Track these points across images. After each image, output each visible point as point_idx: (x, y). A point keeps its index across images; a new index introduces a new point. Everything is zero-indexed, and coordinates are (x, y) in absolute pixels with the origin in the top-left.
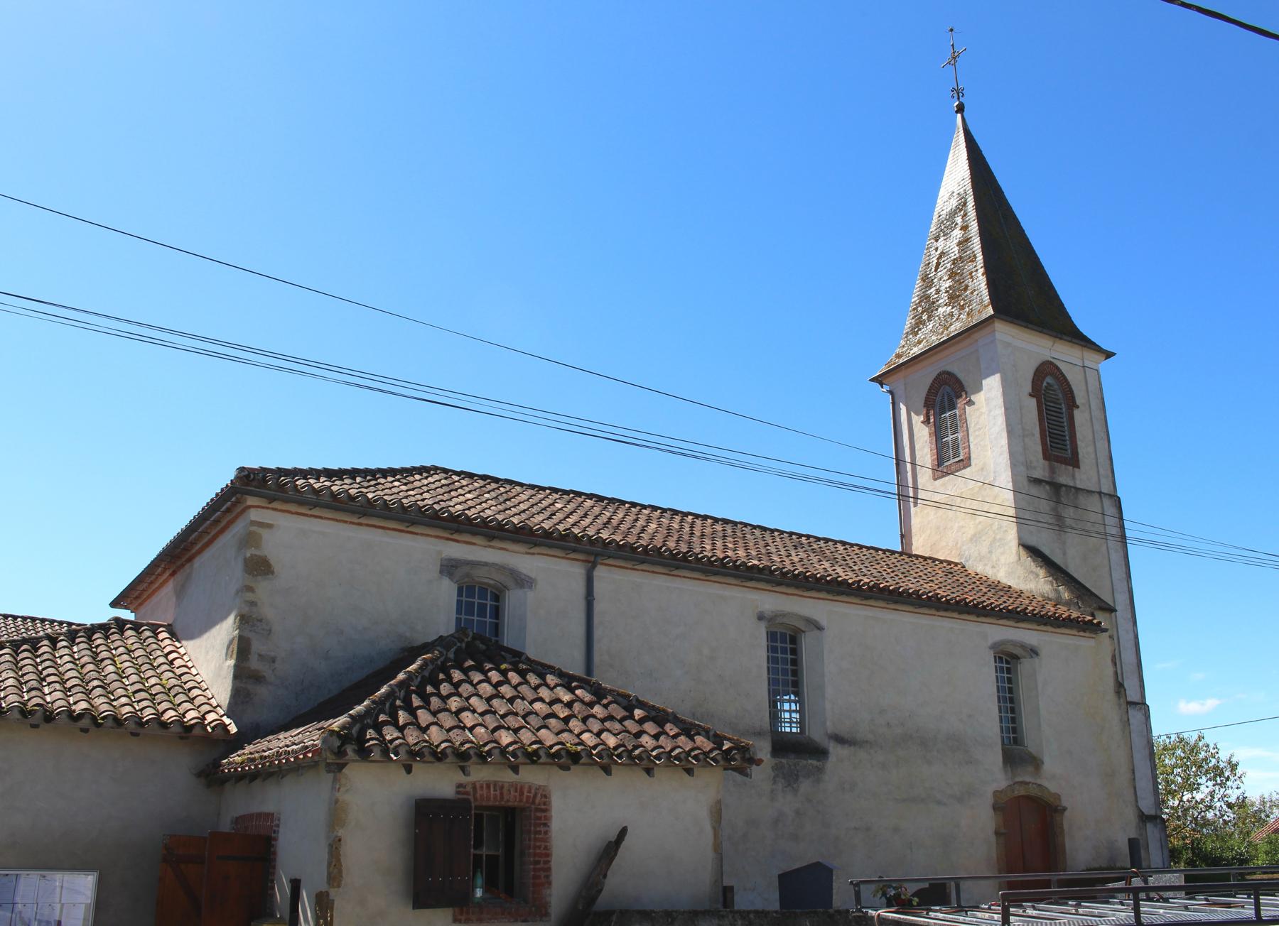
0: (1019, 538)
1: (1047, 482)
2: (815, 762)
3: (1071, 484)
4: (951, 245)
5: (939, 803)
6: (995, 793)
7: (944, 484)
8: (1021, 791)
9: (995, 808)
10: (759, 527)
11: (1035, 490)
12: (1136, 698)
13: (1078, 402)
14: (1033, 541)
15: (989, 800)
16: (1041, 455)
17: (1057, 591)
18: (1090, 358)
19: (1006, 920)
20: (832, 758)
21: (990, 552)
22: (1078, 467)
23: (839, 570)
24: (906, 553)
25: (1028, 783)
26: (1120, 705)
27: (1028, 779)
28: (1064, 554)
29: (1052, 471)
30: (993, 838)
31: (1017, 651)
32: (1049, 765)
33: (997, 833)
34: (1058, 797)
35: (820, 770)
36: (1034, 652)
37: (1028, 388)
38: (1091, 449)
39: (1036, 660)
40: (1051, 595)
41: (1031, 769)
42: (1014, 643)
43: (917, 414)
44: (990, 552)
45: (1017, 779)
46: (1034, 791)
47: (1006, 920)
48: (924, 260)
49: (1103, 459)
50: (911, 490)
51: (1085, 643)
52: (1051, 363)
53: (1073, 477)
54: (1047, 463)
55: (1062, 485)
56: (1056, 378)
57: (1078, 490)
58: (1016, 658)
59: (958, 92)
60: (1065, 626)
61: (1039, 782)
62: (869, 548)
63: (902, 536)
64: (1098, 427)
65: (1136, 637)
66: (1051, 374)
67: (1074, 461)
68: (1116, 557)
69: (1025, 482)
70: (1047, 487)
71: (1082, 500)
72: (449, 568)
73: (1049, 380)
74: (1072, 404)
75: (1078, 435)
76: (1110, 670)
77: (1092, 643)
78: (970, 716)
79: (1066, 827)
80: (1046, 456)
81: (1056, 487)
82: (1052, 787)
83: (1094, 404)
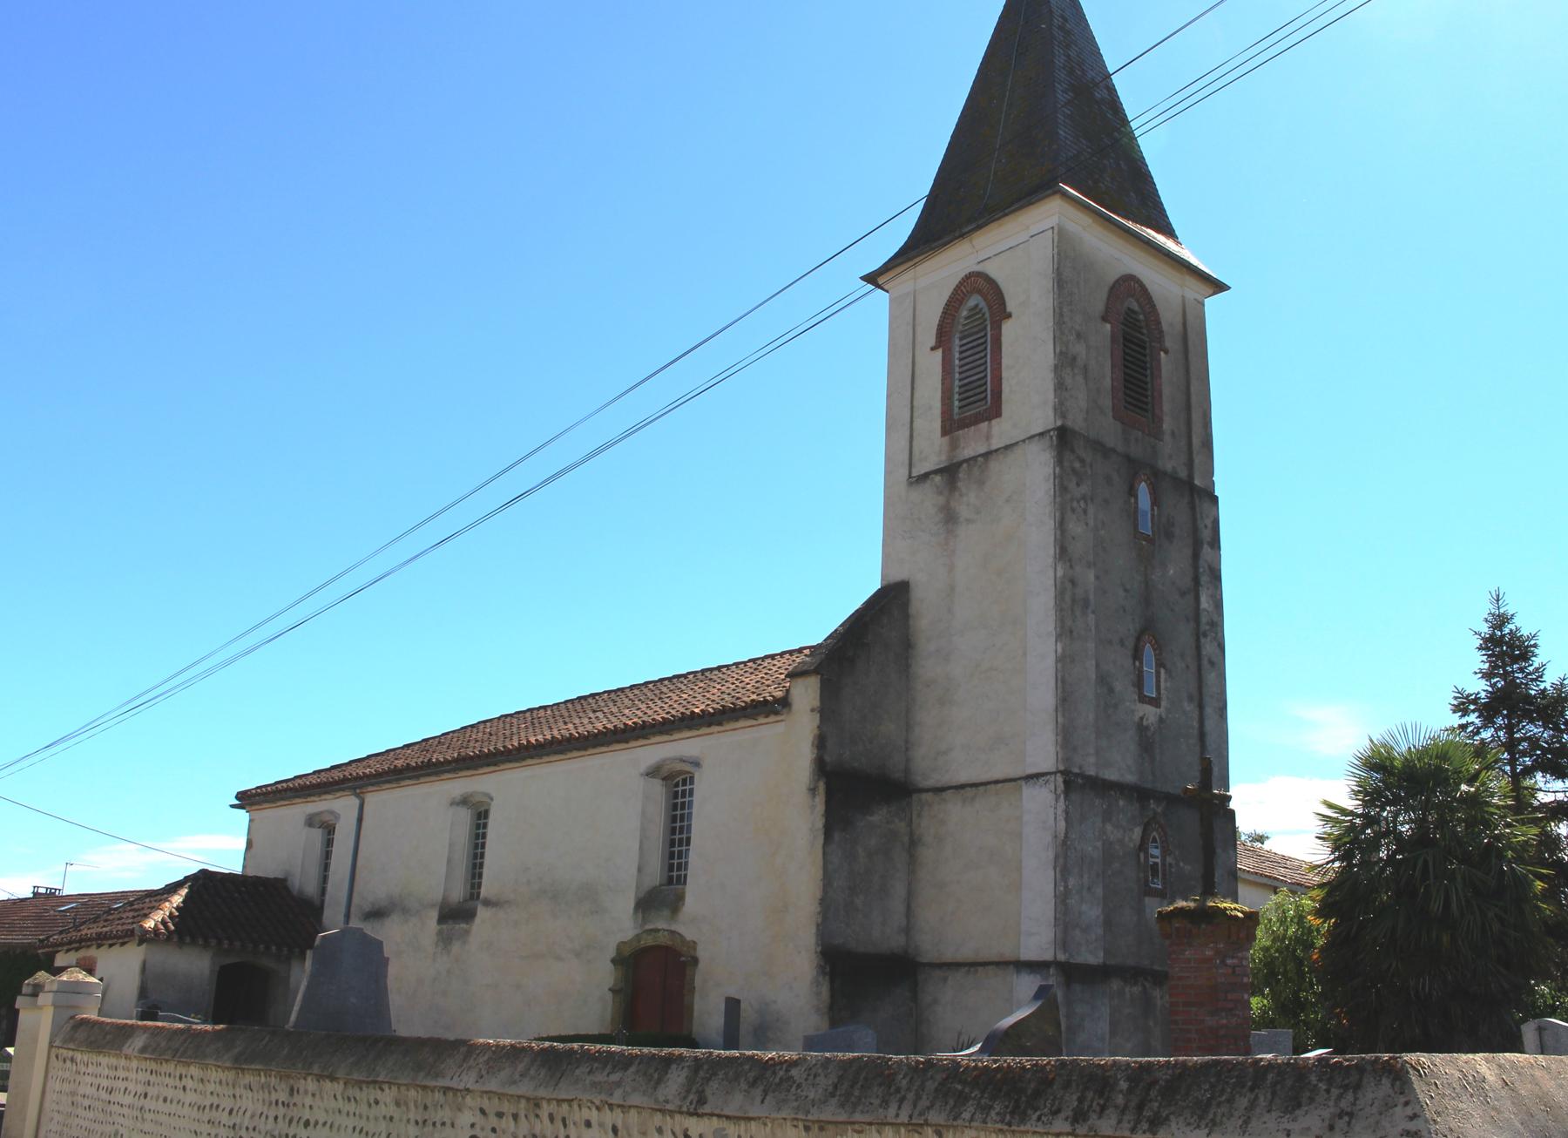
2: (464, 926)
5: (559, 958)
8: (649, 941)
10: (767, 657)
15: (612, 953)
19: (773, 1133)
20: (477, 920)
23: (624, 719)
25: (657, 930)
27: (661, 925)
30: (609, 996)
35: (467, 932)
41: (666, 912)
45: (648, 927)
46: (663, 939)
47: (773, 1133)
60: (679, 729)
62: (782, 654)
66: (979, 292)
72: (310, 821)
73: (974, 300)
77: (780, 728)
82: (688, 933)
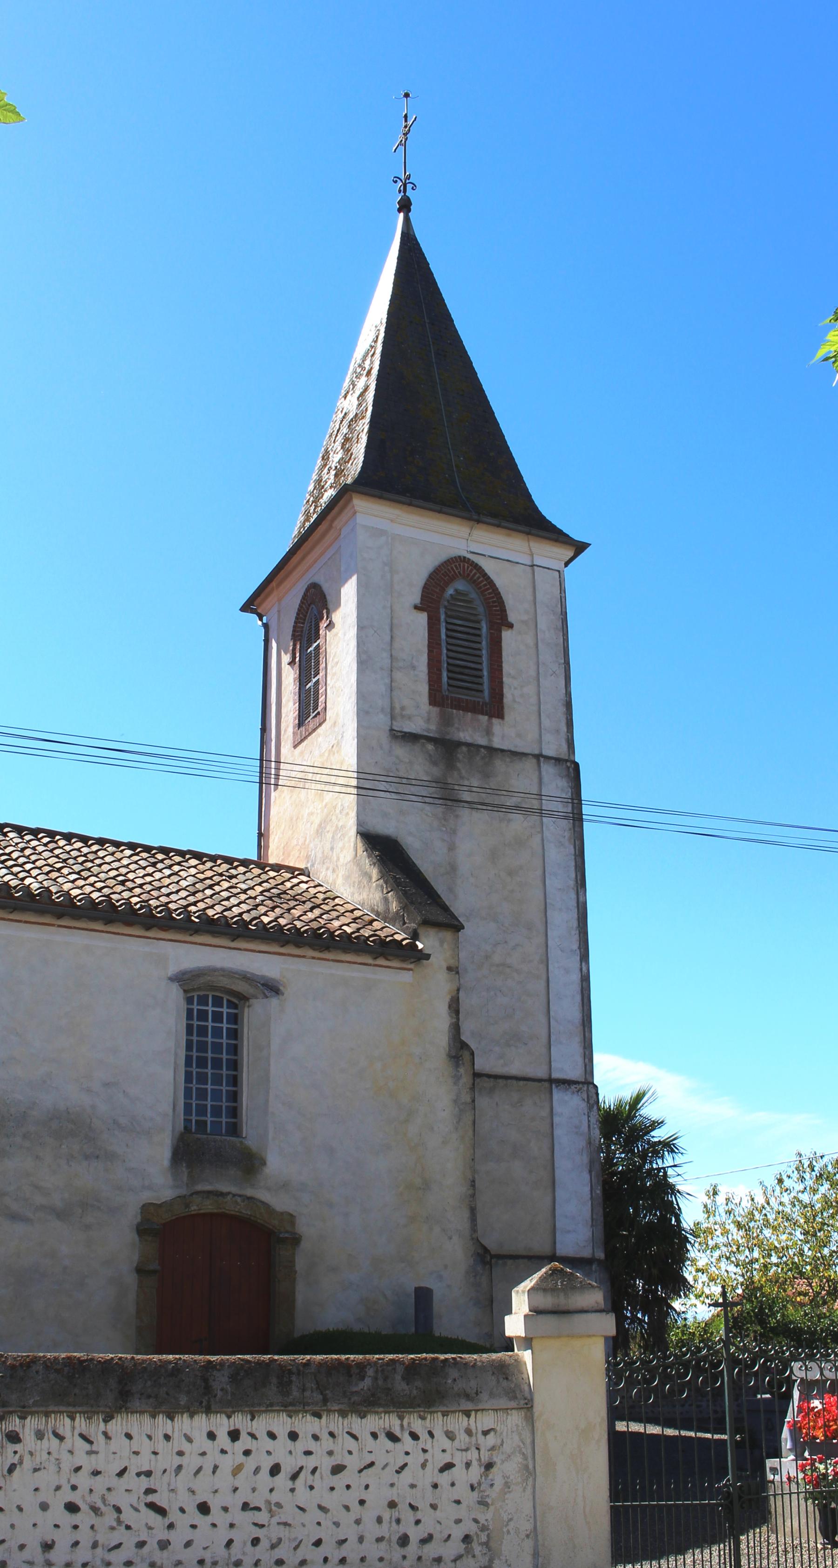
0: (360, 823)
1: (429, 739)
3: (482, 741)
4: (350, 404)
6: (146, 1208)
7: (302, 753)
9: (143, 1230)
11: (401, 751)
12: (574, 1073)
13: (512, 617)
14: (385, 827)
15: (131, 1216)
16: (425, 699)
17: (386, 900)
18: (548, 554)
21: (332, 849)
22: (500, 715)
24: (262, 865)
25: (222, 1194)
26: (457, 1078)
27: (224, 1187)
28: (452, 848)
29: (446, 721)
30: (131, 1280)
31: (241, 987)
32: (276, 1164)
33: (140, 1271)
34: (291, 1218)
36: (272, 988)
37: (416, 597)
38: (530, 690)
39: (274, 1001)
40: (381, 909)
42: (230, 974)
43: (286, 653)
44: (332, 849)
45: (199, 1187)
46: (231, 1207)
48: (330, 431)
49: (552, 704)
50: (273, 764)
51: (391, 978)
52: (464, 560)
53: (489, 732)
54: (435, 710)
55: (460, 744)
56: (473, 582)
57: (492, 751)
58: (244, 998)
59: (406, 183)
61: (249, 1192)
63: (260, 835)
64: (549, 657)
65: (585, 979)
67: (495, 708)
68: (558, 856)
69: (385, 739)
70: (430, 747)
71: (500, 765)
74: (499, 618)
75: (506, 668)
76: (442, 1022)
77: (406, 977)
78: (107, 1085)
79: (300, 1264)
80: (436, 698)
81: (446, 749)
82: (280, 1203)
83: (546, 621)
